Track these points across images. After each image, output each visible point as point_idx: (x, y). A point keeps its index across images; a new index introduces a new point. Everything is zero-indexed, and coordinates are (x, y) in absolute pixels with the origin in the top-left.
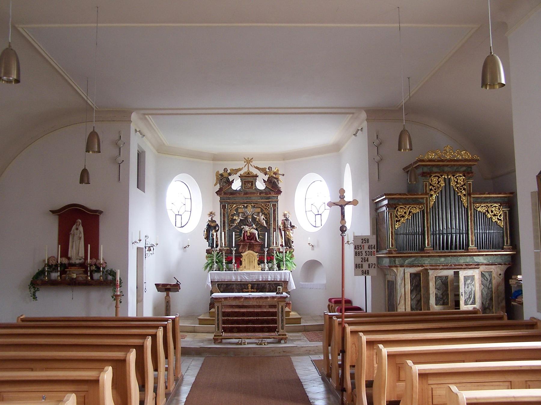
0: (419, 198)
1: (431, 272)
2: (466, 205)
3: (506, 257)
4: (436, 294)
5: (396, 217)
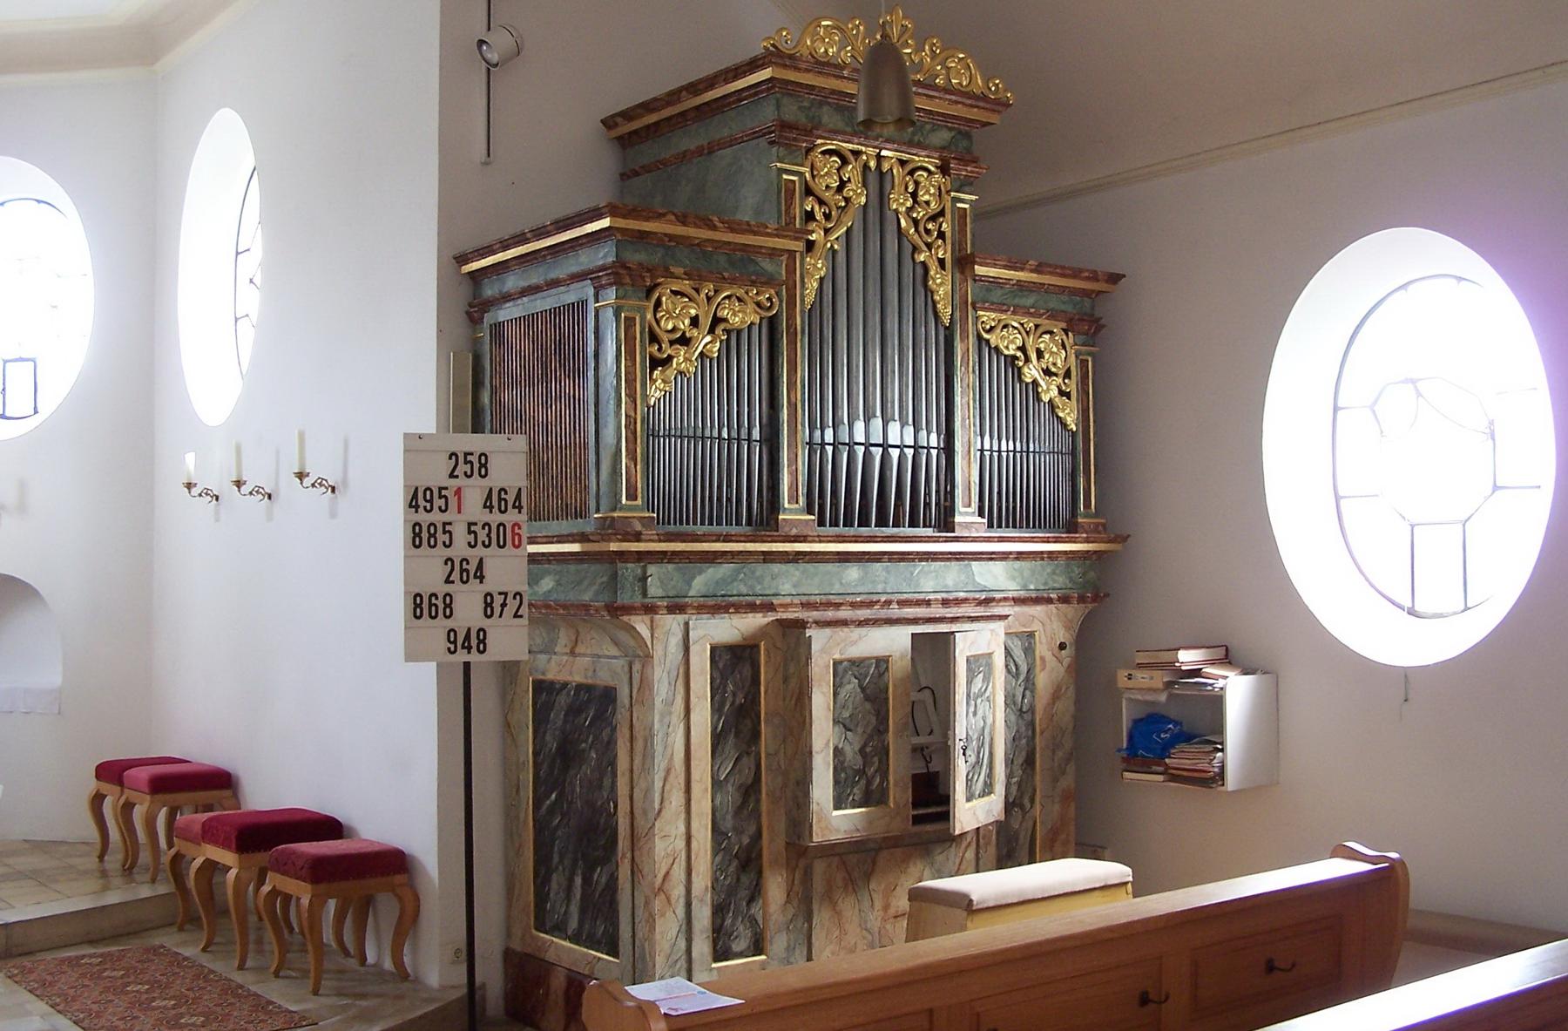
0: (758, 249)
1: (819, 639)
2: (946, 313)
3: (1049, 567)
4: (836, 749)
5: (654, 338)
